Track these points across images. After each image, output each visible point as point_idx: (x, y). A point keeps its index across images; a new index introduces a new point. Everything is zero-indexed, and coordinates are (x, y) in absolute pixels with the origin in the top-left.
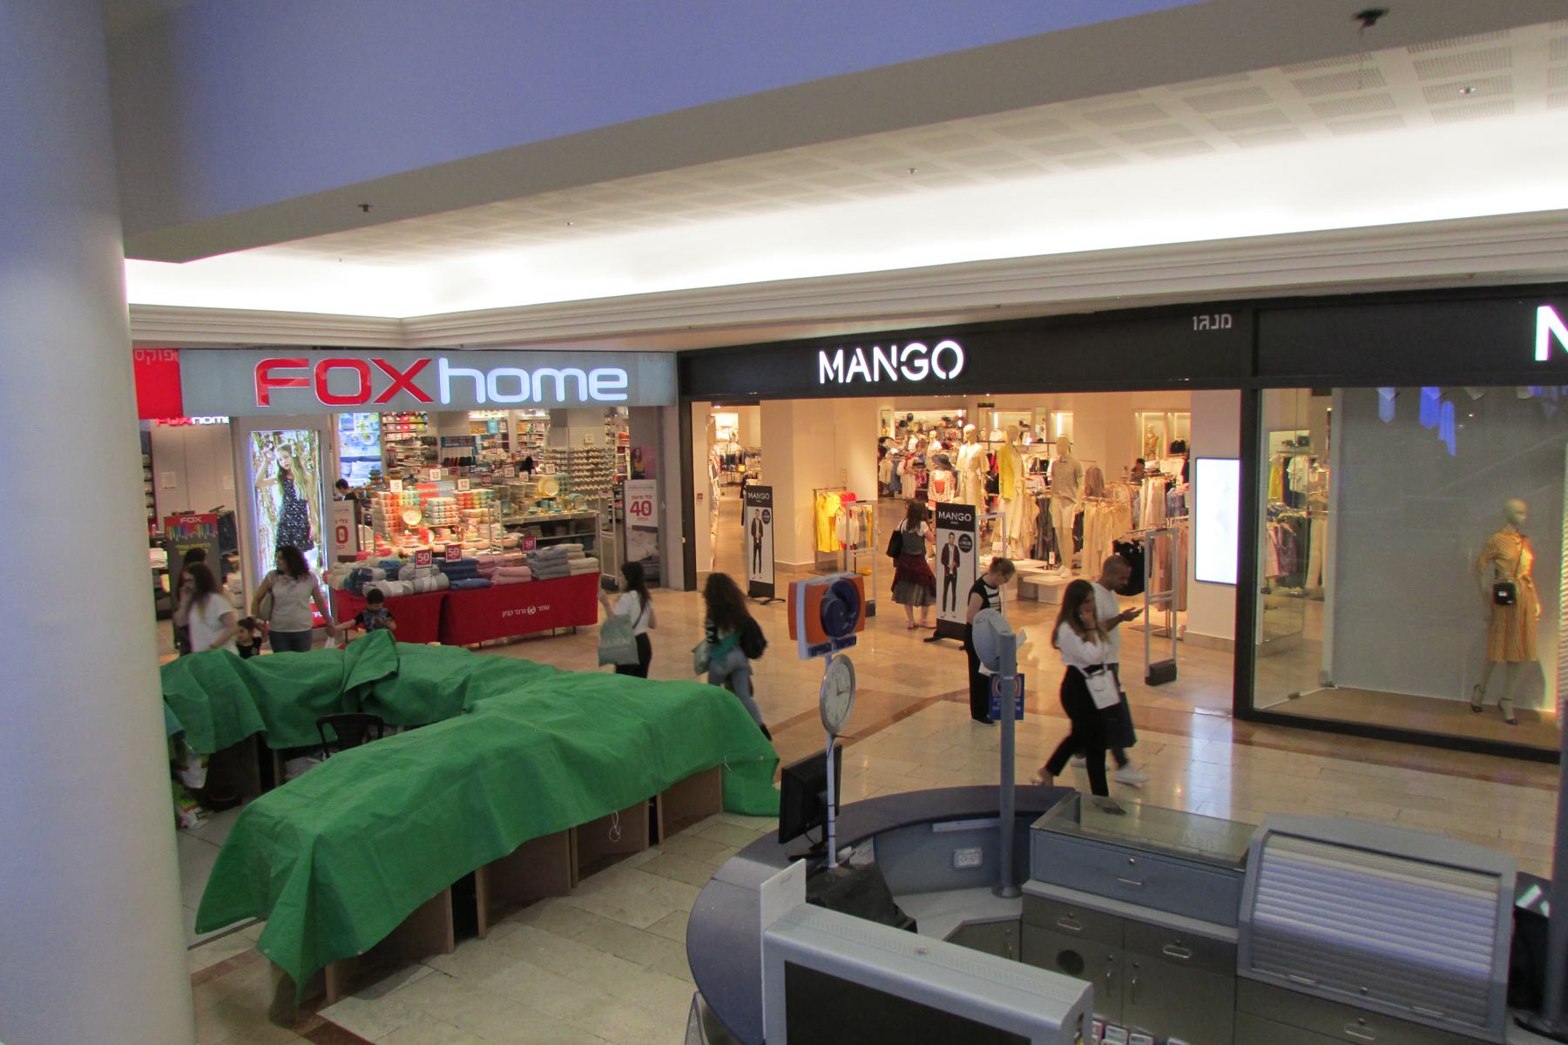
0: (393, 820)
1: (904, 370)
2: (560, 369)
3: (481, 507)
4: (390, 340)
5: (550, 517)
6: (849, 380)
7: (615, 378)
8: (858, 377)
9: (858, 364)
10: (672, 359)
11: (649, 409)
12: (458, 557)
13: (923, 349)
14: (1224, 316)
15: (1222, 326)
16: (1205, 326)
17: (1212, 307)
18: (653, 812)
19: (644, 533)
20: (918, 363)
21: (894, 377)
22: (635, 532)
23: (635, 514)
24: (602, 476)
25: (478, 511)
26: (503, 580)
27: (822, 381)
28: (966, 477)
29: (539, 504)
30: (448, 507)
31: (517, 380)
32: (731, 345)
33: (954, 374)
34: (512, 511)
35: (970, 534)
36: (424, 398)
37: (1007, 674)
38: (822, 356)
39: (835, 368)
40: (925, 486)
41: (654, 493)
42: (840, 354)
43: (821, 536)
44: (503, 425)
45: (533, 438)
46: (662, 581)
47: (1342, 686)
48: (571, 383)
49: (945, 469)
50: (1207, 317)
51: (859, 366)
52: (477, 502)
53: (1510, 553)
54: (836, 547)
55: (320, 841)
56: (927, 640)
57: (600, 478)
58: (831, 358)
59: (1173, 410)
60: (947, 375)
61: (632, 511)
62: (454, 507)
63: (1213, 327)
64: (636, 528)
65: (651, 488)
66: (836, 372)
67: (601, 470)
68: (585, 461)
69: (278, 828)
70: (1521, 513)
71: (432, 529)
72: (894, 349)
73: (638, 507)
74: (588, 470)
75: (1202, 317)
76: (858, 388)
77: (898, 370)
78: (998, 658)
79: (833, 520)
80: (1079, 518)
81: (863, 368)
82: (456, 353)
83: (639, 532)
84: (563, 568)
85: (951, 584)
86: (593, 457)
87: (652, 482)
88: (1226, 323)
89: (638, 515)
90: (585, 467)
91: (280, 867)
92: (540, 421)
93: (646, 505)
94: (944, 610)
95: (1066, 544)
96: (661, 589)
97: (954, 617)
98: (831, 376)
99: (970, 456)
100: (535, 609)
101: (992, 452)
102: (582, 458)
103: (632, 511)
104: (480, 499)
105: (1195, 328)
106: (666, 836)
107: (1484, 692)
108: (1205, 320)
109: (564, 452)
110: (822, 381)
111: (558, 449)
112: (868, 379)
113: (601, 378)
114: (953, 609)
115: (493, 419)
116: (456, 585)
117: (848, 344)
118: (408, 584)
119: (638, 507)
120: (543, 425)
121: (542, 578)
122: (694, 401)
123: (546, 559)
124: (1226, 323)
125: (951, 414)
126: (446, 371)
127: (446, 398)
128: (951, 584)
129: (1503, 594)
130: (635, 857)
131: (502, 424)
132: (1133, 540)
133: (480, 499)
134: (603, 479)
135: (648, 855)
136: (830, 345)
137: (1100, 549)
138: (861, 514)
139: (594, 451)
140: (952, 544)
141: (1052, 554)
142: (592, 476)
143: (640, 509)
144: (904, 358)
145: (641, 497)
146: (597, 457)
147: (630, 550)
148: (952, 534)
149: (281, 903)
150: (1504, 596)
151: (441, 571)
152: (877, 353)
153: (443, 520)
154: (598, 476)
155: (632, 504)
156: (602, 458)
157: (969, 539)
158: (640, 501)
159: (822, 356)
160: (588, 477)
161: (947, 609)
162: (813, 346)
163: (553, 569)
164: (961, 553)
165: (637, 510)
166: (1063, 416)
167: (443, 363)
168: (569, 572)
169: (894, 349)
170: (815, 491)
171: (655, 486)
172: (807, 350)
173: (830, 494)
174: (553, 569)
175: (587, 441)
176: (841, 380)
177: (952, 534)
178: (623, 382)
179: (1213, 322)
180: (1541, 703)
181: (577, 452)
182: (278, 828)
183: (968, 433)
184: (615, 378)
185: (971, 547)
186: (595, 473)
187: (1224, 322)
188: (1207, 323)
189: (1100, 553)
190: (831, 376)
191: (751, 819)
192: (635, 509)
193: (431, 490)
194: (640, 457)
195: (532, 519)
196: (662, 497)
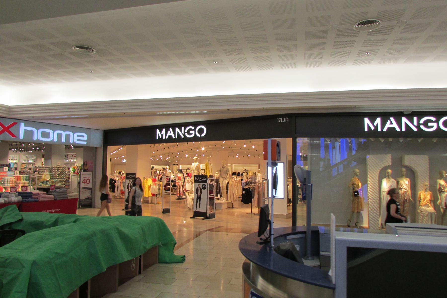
0: (64, 255)
1: (186, 134)
2: (64, 131)
3: (23, 181)
4: (6, 114)
5: (47, 187)
6: (167, 138)
7: (83, 136)
8: (170, 137)
9: (170, 133)
10: (102, 132)
11: (92, 148)
12: (26, 191)
13: (193, 128)
14: (286, 118)
15: (286, 121)
16: (281, 121)
17: (283, 116)
18: (140, 260)
19: (86, 190)
20: (191, 132)
21: (183, 136)
22: (83, 189)
23: (84, 183)
24: (63, 176)
25: (22, 182)
26: (43, 199)
27: (157, 138)
28: (194, 172)
29: (43, 183)
30: (11, 180)
31: (49, 133)
32: (125, 127)
33: (203, 135)
34: (33, 184)
35: (206, 184)
36: (13, 135)
37: (309, 184)
38: (158, 131)
39: (162, 134)
40: (169, 181)
41: (91, 176)
42: (164, 130)
43: (145, 192)
44: (15, 165)
45: (27, 169)
46: (93, 206)
47: (313, 223)
48: (68, 136)
49: (181, 173)
50: (281, 119)
51: (170, 133)
52: (22, 179)
53: (356, 183)
54: (150, 195)
55: (34, 263)
56: (191, 218)
57: (62, 177)
58: (161, 131)
59: (233, 164)
60: (201, 136)
61: (83, 182)
62: (14, 180)
63: (283, 121)
64: (84, 188)
65: (90, 175)
66: (162, 136)
67: (62, 174)
68: (57, 171)
69: (8, 261)
70: (358, 172)
71: (4, 187)
72: (183, 128)
73: (85, 181)
74: (57, 174)
75: (280, 119)
76: (170, 140)
77: (184, 135)
78: (305, 179)
79: (149, 187)
80: (228, 183)
81: (172, 134)
82: (27, 122)
83: (85, 189)
84: (65, 196)
85: (199, 200)
86: (60, 170)
87: (91, 173)
88: (287, 120)
89: (85, 183)
90: (57, 173)
91: (9, 278)
92: (30, 163)
93: (88, 180)
94: (196, 208)
95: (224, 192)
96: (92, 208)
97: (200, 210)
98: (161, 137)
99: (195, 166)
100: (54, 210)
101: (188, 173)
102: (56, 170)
103: (83, 182)
104: (23, 178)
105: (278, 122)
106: (144, 270)
107: (350, 221)
108: (281, 119)
109: (49, 168)
110: (157, 138)
111: (47, 166)
112: (174, 137)
113: (78, 136)
114: (199, 208)
115: (12, 162)
116: (25, 200)
117: (167, 127)
118: (5, 199)
119: (85, 181)
120: (32, 165)
121: (58, 199)
122: (108, 146)
123: (60, 193)
124: (287, 120)
125: (165, 167)
126: (23, 127)
127: (22, 136)
128: (199, 200)
129: (356, 194)
130: (135, 278)
131: (15, 164)
132: (248, 187)
133: (23, 178)
134: (63, 177)
135: (137, 278)
136: (161, 127)
137: (233, 193)
138: (159, 185)
139: (60, 168)
140: (199, 187)
141: (219, 195)
142: (59, 176)
143: (86, 181)
144: (186, 131)
145: (87, 178)
146: (61, 170)
147: (81, 195)
148: (199, 184)
149: (16, 292)
150: (356, 194)
151: (19, 195)
152: (177, 130)
153: (9, 185)
154: (61, 176)
155: (83, 180)
156: (63, 170)
157: (205, 185)
158: (86, 179)
159: (158, 131)
160: (57, 176)
161: (197, 208)
162: (154, 128)
163: (63, 196)
164: (203, 190)
165: (85, 182)
166: (202, 165)
167: (22, 125)
168: (68, 198)
169: (183, 128)
170: (144, 178)
171: (92, 174)
172: (153, 129)
173: (149, 178)
174: (63, 196)
175: (58, 164)
176: (164, 138)
177: (199, 184)
178: (86, 138)
179: (283, 120)
180: (362, 224)
181: (55, 168)
182: (8, 261)
183: (195, 159)
184: (83, 136)
185: (206, 188)
186: (60, 175)
187: (286, 120)
188: (281, 120)
189: (233, 194)
190: (161, 137)
191: (170, 264)
192: (84, 181)
193: (4, 174)
194: (87, 164)
195: (40, 187)
196: (94, 177)
